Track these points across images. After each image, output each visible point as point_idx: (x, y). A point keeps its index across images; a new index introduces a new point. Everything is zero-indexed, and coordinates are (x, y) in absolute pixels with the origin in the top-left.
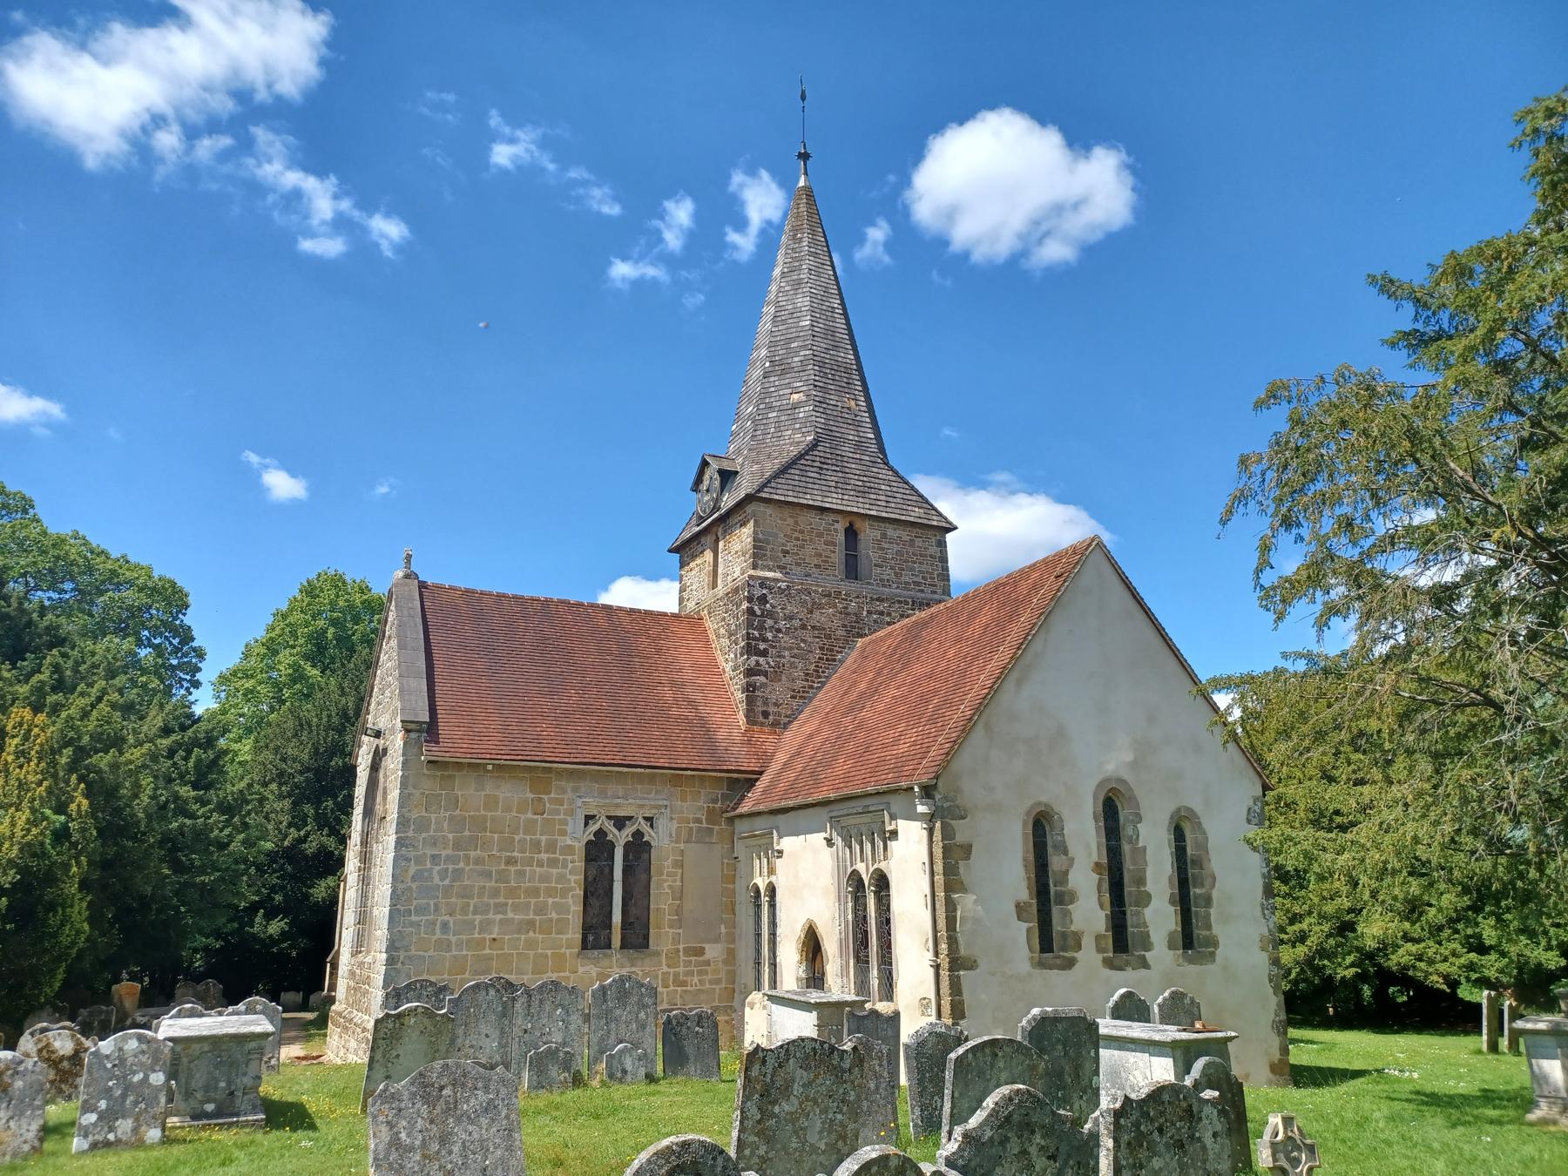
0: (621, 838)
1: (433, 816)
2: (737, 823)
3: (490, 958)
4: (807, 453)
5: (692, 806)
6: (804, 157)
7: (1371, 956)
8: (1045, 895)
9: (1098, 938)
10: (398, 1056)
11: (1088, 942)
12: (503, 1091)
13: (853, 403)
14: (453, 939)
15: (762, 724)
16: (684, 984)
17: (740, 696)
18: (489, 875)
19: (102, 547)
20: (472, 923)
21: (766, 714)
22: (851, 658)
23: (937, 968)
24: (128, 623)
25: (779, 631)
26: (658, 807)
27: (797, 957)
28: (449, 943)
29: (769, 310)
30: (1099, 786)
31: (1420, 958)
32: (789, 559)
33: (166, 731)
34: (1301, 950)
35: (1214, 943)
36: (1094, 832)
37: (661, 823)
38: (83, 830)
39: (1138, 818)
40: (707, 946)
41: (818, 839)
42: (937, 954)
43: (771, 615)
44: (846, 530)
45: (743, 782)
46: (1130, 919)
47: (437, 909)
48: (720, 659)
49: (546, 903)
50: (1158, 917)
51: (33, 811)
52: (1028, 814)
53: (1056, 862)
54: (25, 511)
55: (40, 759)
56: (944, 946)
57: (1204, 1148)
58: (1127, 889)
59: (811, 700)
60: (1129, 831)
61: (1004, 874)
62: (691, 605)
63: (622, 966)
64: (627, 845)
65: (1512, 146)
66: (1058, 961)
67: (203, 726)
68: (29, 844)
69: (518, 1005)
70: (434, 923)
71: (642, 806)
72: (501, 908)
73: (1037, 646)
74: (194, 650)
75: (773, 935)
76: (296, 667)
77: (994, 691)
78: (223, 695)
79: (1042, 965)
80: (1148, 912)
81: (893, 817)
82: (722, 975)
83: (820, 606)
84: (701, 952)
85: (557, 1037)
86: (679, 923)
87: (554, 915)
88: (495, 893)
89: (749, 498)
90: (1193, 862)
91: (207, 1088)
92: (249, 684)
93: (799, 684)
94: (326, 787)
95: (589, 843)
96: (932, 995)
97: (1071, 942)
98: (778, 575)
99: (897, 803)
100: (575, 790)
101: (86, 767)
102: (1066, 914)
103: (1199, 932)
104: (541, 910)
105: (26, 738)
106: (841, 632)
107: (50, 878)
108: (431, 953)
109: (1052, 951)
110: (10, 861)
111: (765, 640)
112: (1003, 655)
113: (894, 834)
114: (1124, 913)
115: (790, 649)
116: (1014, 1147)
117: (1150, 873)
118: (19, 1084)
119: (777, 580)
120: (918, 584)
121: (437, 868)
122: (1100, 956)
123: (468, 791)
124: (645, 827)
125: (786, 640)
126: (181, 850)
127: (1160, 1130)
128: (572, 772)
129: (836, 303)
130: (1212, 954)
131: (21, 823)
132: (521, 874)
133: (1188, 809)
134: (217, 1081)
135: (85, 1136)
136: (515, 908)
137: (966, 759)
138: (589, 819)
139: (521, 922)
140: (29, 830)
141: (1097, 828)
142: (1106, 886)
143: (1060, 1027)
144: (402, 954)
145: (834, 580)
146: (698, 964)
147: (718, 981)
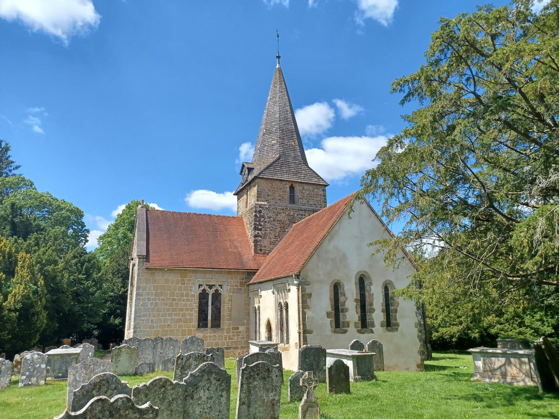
0: (211, 292)
2: (250, 286)
3: (167, 331)
4: (276, 161)
5: (235, 281)
6: (278, 57)
7: (486, 330)
8: (337, 309)
9: (355, 323)
11: (352, 325)
12: (108, 367)
13: (293, 143)
14: (155, 325)
15: (260, 253)
16: (232, 339)
17: (253, 244)
18: (167, 304)
19: (57, 197)
20: (161, 320)
21: (261, 250)
22: (290, 230)
23: (300, 333)
24: (63, 222)
25: (266, 222)
26: (223, 282)
27: (265, 330)
29: (266, 111)
30: (357, 274)
31: (502, 330)
32: (270, 197)
33: (75, 257)
34: (460, 327)
35: (397, 325)
37: (224, 287)
38: (42, 291)
39: (371, 284)
41: (270, 291)
42: (300, 328)
43: (263, 217)
45: (251, 273)
46: (368, 317)
48: (247, 232)
50: (378, 316)
51: (26, 285)
52: (331, 283)
53: (341, 299)
54: (31, 186)
55: (28, 268)
56: (301, 326)
57: (272, 379)
58: (367, 308)
59: (277, 245)
61: (323, 303)
63: (211, 333)
64: (213, 294)
67: (87, 256)
68: (24, 295)
69: (159, 345)
70: (148, 320)
71: (217, 281)
72: (170, 315)
73: (337, 228)
74: (86, 230)
76: (124, 233)
77: (320, 243)
78: (101, 243)
79: (335, 332)
80: (374, 315)
81: (289, 285)
82: (245, 336)
83: (280, 213)
84: (238, 328)
85: (171, 355)
86: (230, 319)
87: (188, 317)
88: (168, 310)
89: (255, 178)
91: (59, 369)
92: (109, 239)
93: (273, 240)
94: (125, 277)
95: (200, 294)
96: (298, 342)
97: (346, 324)
98: (266, 203)
99: (290, 280)
100: (195, 276)
101: (44, 270)
103: (393, 321)
104: (184, 315)
105: (24, 262)
106: (287, 222)
107: (32, 306)
108: (148, 329)
110: (19, 300)
111: (261, 225)
112: (324, 232)
113: (289, 290)
115: (270, 228)
116: (206, 377)
117: (375, 302)
118: (3, 367)
119: (265, 205)
120: (315, 204)
122: (356, 329)
123: (159, 276)
124: (219, 288)
125: (268, 225)
126: (80, 296)
127: (258, 374)
128: (194, 271)
129: (288, 108)
130: (397, 329)
131: (21, 289)
132: (177, 304)
133: (390, 281)
134: (62, 367)
135: (22, 382)
136: (175, 315)
137: (310, 265)
138: (200, 286)
140: (24, 291)
141: (356, 287)
142: (359, 306)
143: (312, 351)
144: (138, 330)
145: (286, 203)
146: (237, 332)
147: (243, 338)
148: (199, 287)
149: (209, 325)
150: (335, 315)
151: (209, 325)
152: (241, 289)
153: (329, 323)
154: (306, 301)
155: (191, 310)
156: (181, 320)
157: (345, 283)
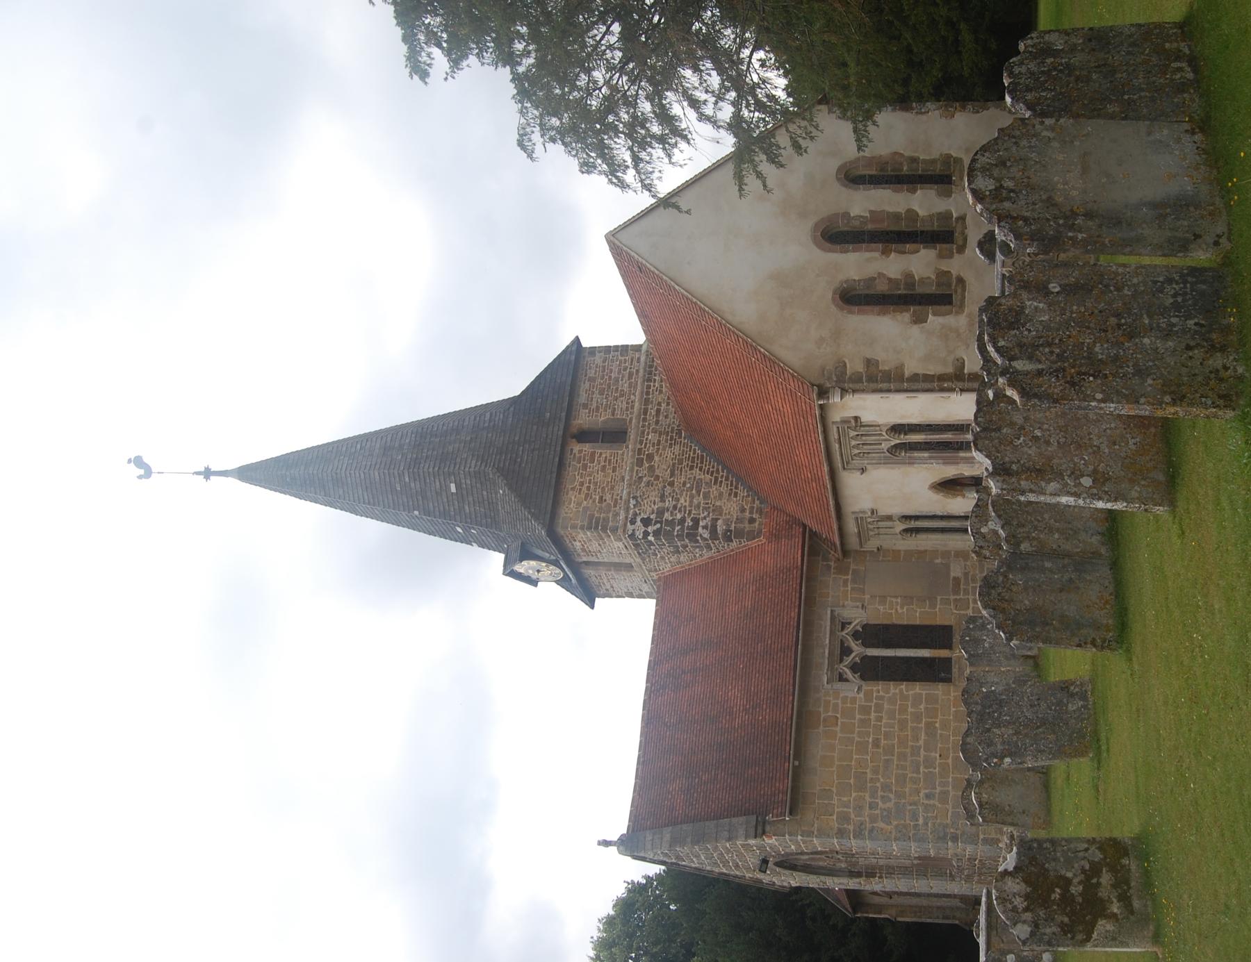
0: (857, 649)
9: (941, 256)
11: (945, 266)
14: (938, 789)
23: (962, 390)
25: (675, 507)
27: (959, 499)
28: (942, 792)
32: (608, 497)
40: (952, 575)
47: (915, 804)
50: (923, 203)
52: (842, 309)
53: (882, 287)
58: (904, 229)
60: (857, 223)
64: (865, 645)
65: (446, 79)
66: (959, 291)
70: (926, 807)
72: (915, 751)
75: (942, 518)
80: (922, 213)
83: (651, 469)
84: (957, 580)
88: (902, 756)
90: (882, 170)
95: (863, 678)
102: (922, 280)
108: (950, 807)
111: (683, 521)
114: (922, 232)
115: (692, 497)
117: (891, 209)
120: (631, 375)
122: (956, 256)
132: (887, 735)
142: (900, 246)
145: (626, 454)
146: (967, 583)
148: (847, 680)
149: (943, 653)
150: (920, 304)
151: (943, 653)
152: (854, 571)
153: (940, 320)
154: (884, 372)
155: (904, 698)
156: (929, 726)
157: (841, 277)
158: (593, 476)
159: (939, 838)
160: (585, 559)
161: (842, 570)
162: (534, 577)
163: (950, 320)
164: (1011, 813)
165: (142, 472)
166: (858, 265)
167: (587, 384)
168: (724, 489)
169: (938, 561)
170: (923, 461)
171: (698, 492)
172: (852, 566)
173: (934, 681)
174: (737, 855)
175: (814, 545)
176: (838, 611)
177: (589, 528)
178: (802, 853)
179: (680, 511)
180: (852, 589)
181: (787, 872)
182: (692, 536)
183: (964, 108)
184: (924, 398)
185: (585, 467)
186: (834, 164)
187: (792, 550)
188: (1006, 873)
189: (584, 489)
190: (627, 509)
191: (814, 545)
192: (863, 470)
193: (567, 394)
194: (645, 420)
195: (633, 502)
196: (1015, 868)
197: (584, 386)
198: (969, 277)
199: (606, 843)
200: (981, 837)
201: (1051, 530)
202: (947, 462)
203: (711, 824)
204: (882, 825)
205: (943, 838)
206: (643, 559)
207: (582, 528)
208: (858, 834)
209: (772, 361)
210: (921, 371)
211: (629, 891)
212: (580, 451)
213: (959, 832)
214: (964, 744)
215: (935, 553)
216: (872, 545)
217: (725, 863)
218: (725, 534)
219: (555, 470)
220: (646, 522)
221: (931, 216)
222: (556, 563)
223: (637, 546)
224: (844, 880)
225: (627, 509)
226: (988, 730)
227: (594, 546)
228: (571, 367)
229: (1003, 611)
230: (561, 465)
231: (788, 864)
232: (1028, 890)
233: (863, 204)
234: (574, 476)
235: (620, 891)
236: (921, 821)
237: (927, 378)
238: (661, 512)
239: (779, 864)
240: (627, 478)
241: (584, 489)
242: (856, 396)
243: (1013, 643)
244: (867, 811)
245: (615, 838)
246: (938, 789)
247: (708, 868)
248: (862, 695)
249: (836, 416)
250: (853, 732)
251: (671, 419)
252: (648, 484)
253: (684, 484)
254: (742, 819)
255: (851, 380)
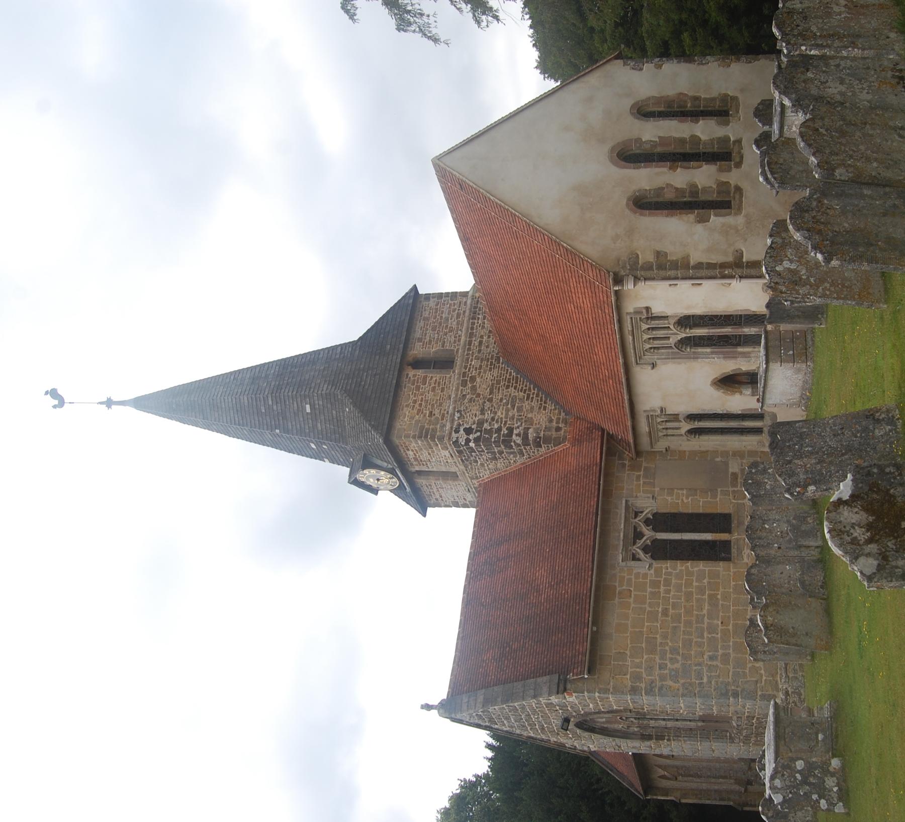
0: (648, 533)
1: (630, 670)
9: (721, 170)
10: (793, 628)
11: (724, 178)
14: (721, 652)
23: (741, 277)
25: (493, 419)
27: (737, 396)
28: (724, 655)
32: (436, 412)
36: (648, 169)
39: (638, 140)
40: (731, 470)
44: (414, 368)
47: (699, 664)
49: (697, 587)
50: (705, 131)
53: (669, 196)
60: (648, 146)
61: (680, 234)
62: (470, 497)
64: (655, 530)
66: (737, 196)
72: (700, 619)
79: (740, 209)
83: (474, 388)
84: (734, 475)
88: (688, 623)
90: (669, 107)
95: (653, 557)
102: (704, 189)
108: (731, 667)
109: (730, 202)
111: (499, 430)
115: (507, 410)
117: (677, 135)
120: (458, 315)
121: (669, 665)
122: (734, 170)
127: (798, 26)
132: (674, 606)
139: (710, 604)
142: (685, 164)
145: (453, 377)
149: (724, 536)
151: (724, 536)
152: (646, 468)
153: (721, 220)
154: (672, 262)
157: (634, 187)
158: (423, 395)
159: (722, 694)
160: (417, 468)
161: (635, 467)
162: (375, 486)
163: (730, 220)
164: (794, 635)
165: (56, 402)
166: (647, 178)
167: (422, 323)
168: (534, 404)
169: (718, 459)
170: (706, 356)
171: (513, 407)
172: (644, 464)
173: (716, 560)
174: (544, 715)
175: (611, 447)
176: (631, 501)
177: (420, 437)
178: (600, 712)
179: (497, 422)
180: (644, 483)
181: (586, 734)
182: (507, 442)
183: (738, 60)
184: (709, 286)
185: (418, 388)
186: (628, 103)
187: (593, 450)
188: (840, 502)
189: (417, 406)
190: (453, 421)
191: (611, 447)
192: (654, 366)
193: (405, 329)
194: (469, 349)
195: (457, 415)
196: (852, 496)
197: (420, 324)
198: (745, 185)
199: (428, 707)
200: (759, 693)
201: (868, 160)
202: (727, 356)
203: (519, 685)
204: (670, 683)
205: (725, 695)
206: (466, 467)
207: (414, 437)
208: (650, 691)
209: (572, 254)
210: (704, 260)
211: (462, 787)
212: (414, 376)
213: (739, 689)
214: (749, 574)
215: (715, 453)
216: (661, 446)
217: (532, 725)
218: (535, 441)
219: (393, 390)
220: (468, 431)
221: (712, 140)
222: (392, 472)
223: (460, 452)
224: (637, 743)
225: (453, 421)
226: (790, 462)
227: (424, 455)
228: (410, 308)
229: (819, 232)
230: (398, 386)
231: (587, 725)
232: (871, 519)
233: (651, 132)
234: (408, 395)
235: (454, 788)
236: (705, 680)
237: (711, 266)
238: (481, 423)
239: (579, 725)
240: (453, 396)
241: (417, 406)
242: (648, 283)
243: (835, 263)
244: (657, 672)
245: (435, 702)
246: (721, 652)
247: (518, 732)
248: (652, 571)
249: (630, 306)
250: (645, 603)
251: (491, 347)
252: (471, 400)
253: (501, 400)
254: (546, 678)
255: (643, 268)
